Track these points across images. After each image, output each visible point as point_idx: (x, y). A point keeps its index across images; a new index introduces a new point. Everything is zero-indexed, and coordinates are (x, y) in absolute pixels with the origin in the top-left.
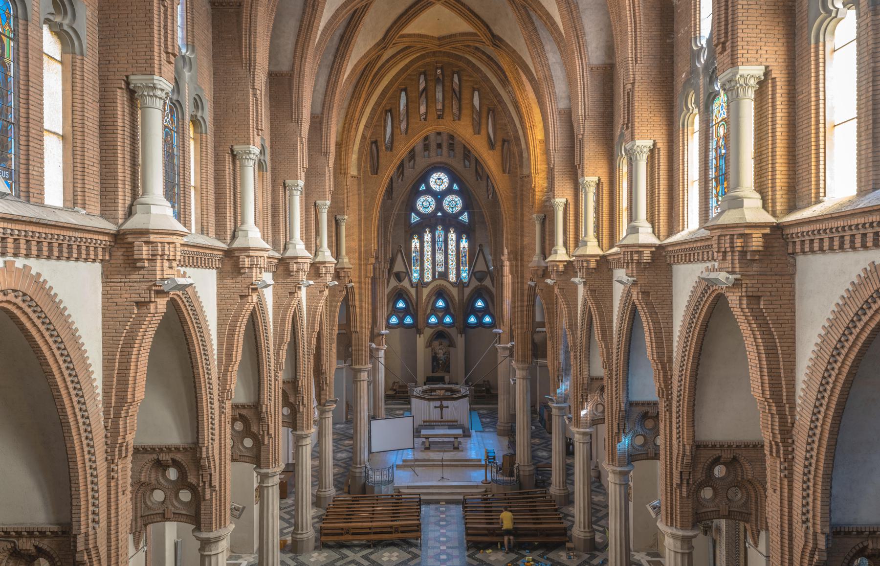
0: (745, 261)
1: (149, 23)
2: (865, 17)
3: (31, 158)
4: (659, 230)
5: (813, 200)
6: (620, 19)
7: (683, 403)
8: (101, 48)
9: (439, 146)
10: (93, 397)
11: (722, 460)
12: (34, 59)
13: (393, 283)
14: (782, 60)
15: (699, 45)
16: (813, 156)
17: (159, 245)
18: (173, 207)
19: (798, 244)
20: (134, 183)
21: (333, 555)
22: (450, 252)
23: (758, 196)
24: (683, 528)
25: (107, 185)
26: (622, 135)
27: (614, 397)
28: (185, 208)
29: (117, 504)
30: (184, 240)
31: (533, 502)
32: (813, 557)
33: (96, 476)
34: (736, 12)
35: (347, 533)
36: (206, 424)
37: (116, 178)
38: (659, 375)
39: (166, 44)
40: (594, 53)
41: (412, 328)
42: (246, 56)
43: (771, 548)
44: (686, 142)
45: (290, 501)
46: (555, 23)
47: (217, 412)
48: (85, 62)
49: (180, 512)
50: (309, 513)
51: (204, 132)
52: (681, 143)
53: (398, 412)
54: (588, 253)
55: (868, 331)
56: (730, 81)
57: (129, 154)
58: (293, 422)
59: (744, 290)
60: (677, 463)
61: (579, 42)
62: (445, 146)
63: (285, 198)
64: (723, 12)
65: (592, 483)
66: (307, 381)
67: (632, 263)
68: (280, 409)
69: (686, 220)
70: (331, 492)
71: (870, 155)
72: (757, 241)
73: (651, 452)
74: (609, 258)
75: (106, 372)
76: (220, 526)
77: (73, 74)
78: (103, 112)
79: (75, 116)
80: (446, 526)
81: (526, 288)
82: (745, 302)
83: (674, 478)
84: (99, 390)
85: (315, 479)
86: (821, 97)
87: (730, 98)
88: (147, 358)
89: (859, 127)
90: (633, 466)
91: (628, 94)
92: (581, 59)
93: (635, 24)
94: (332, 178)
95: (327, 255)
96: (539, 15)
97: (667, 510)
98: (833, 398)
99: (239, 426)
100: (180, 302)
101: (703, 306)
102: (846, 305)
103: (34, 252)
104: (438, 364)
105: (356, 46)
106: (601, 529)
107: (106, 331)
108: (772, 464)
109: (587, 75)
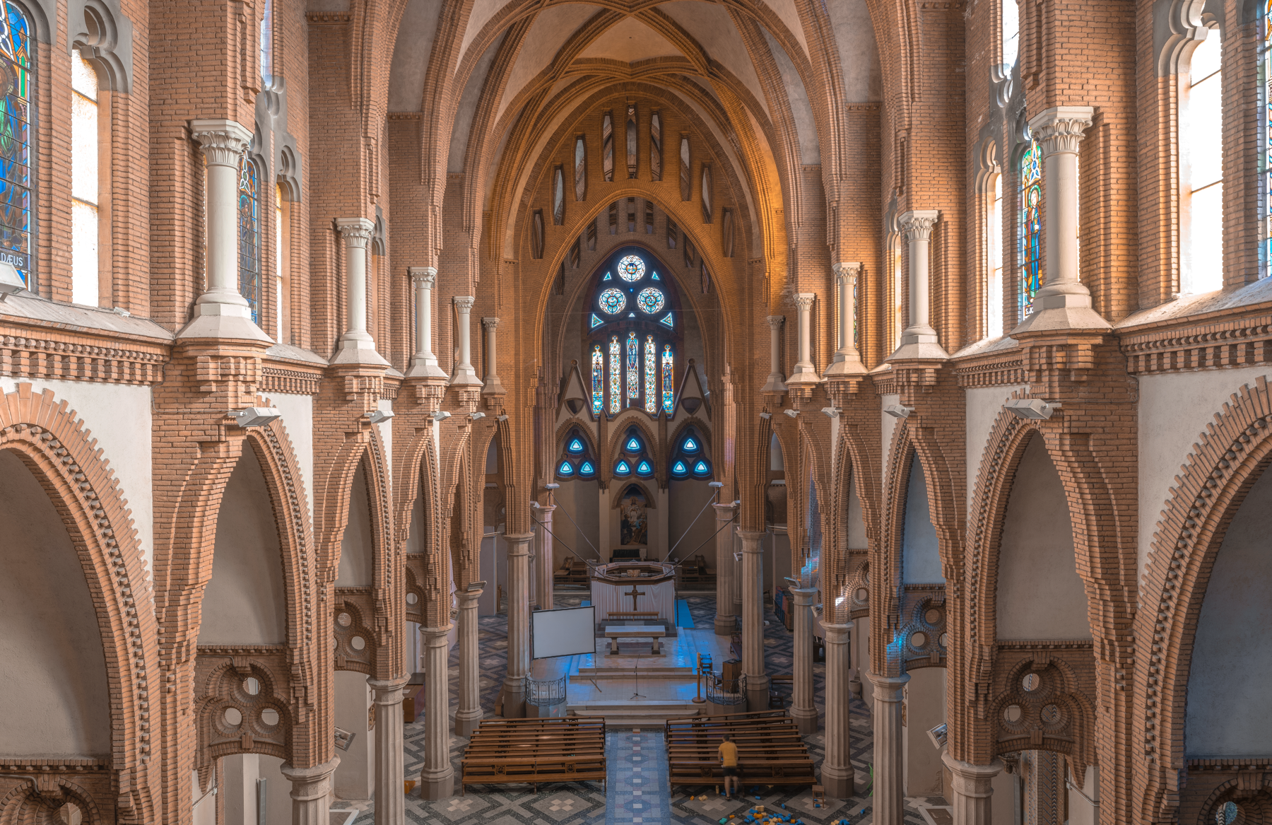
0: (1068, 384)
1: (220, 46)
2: (1233, 39)
3: (54, 238)
4: (947, 340)
5: (1162, 296)
6: (890, 39)
7: (981, 585)
8: (152, 82)
9: (632, 217)
10: (140, 576)
11: (1034, 666)
12: (60, 98)
13: (565, 414)
14: (1118, 99)
15: (1001, 76)
16: (1162, 235)
17: (232, 360)
18: (251, 306)
19: (1142, 359)
20: (198, 273)
21: (480, 802)
22: (647, 370)
23: (1085, 291)
24: (978, 762)
25: (160, 276)
26: (894, 202)
27: (883, 578)
28: (268, 308)
29: (175, 729)
30: (267, 353)
31: (765, 728)
32: (1160, 802)
33: (146, 689)
34: (1053, 30)
35: (500, 772)
36: (298, 616)
37: (172, 265)
38: (947, 546)
39: (244, 76)
40: (853, 86)
41: (592, 479)
42: (356, 91)
43: (1101, 789)
44: (984, 213)
45: (418, 726)
46: (797, 43)
47: (313, 599)
48: (130, 103)
49: (263, 740)
50: (445, 744)
51: (295, 199)
52: (977, 214)
53: (572, 601)
54: (846, 371)
55: (1239, 482)
56: (1045, 128)
57: (190, 231)
58: (422, 613)
59: (1066, 424)
60: (971, 671)
61: (831, 71)
62: (640, 217)
63: (410, 293)
64: (1034, 30)
65: (851, 701)
66: (441, 555)
67: (909, 386)
68: (404, 595)
69: (985, 325)
70: (477, 714)
71: (1242, 234)
72: (1084, 355)
73: (935, 657)
74: (876, 379)
75: (158, 542)
76: (320, 760)
77: (113, 119)
78: (154, 172)
79: (115, 179)
80: (641, 762)
81: (757, 422)
82: (1067, 442)
83: (967, 692)
84: (149, 567)
85: (455, 696)
86: (1173, 151)
87: (1045, 153)
88: (216, 521)
89: (1225, 195)
90: (909, 677)
91: (902, 143)
92: (835, 94)
93: (911, 46)
94: (477, 263)
95: (469, 374)
96: (774, 32)
97: (955, 738)
98: (1190, 578)
99: (345, 619)
100: (261, 442)
101: (1009, 448)
102: (1208, 447)
103: (58, 371)
104: (630, 531)
105: (512, 76)
106: (863, 766)
107: (158, 483)
108: (1104, 671)
109: (843, 117)
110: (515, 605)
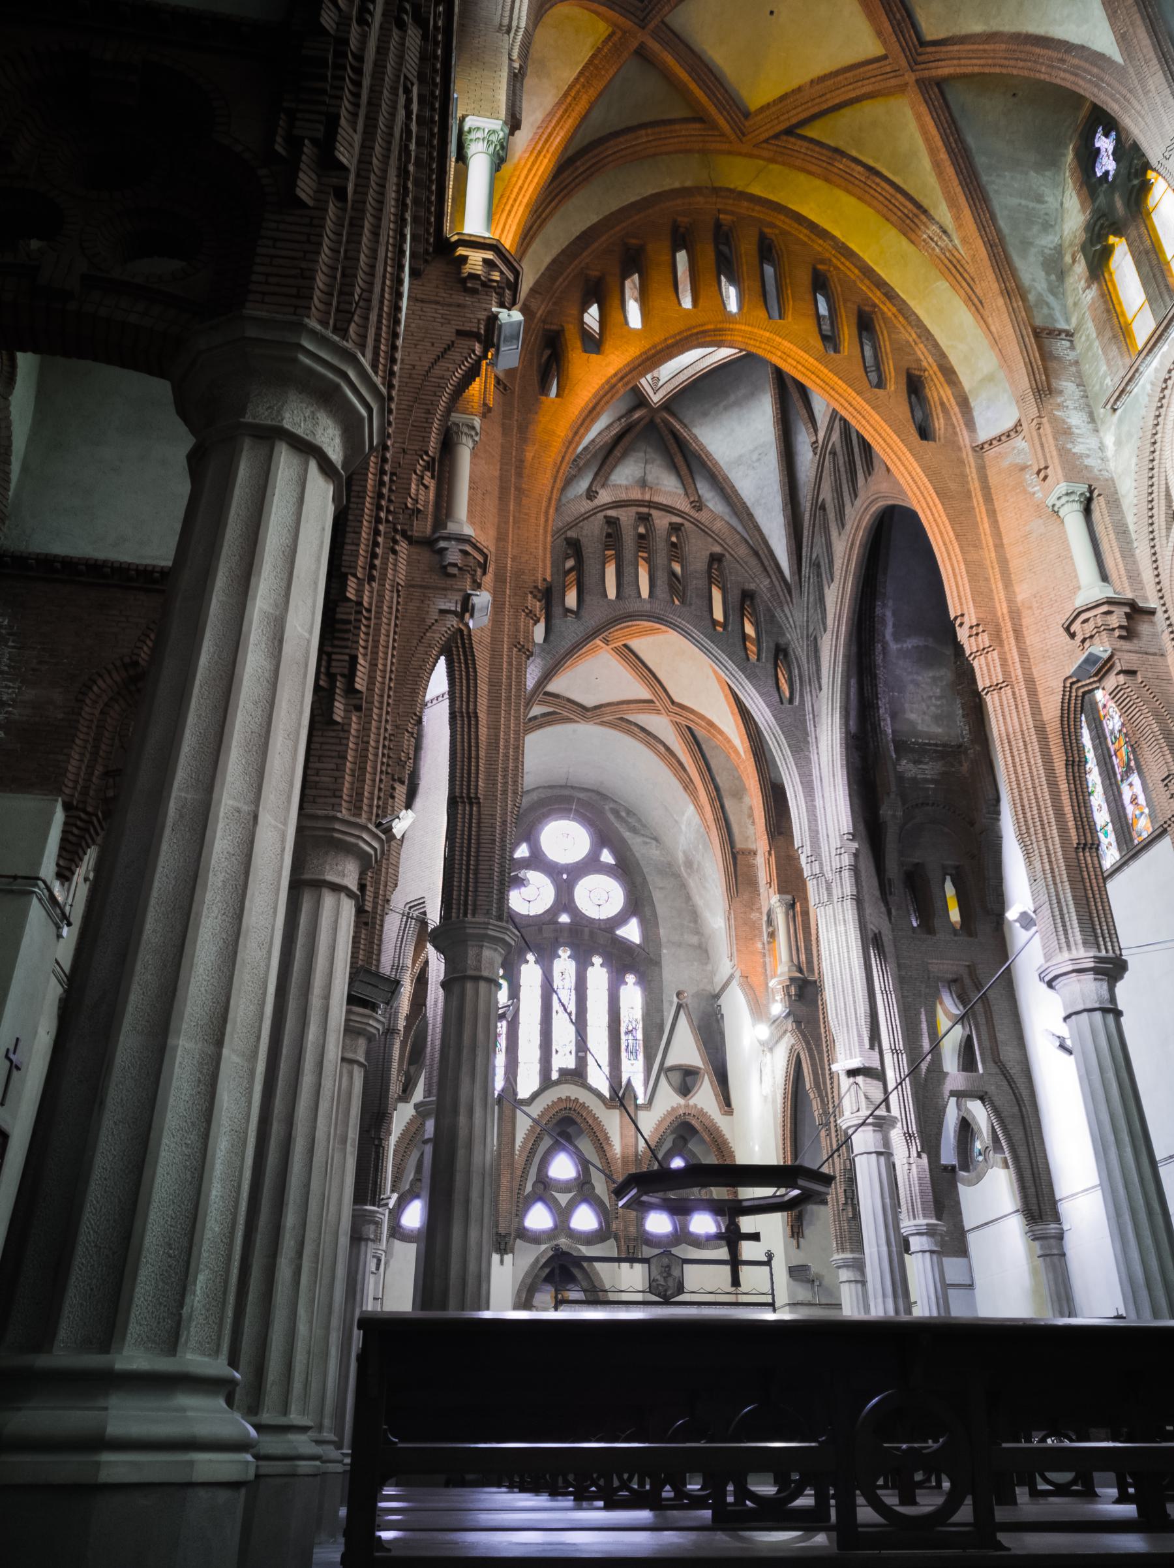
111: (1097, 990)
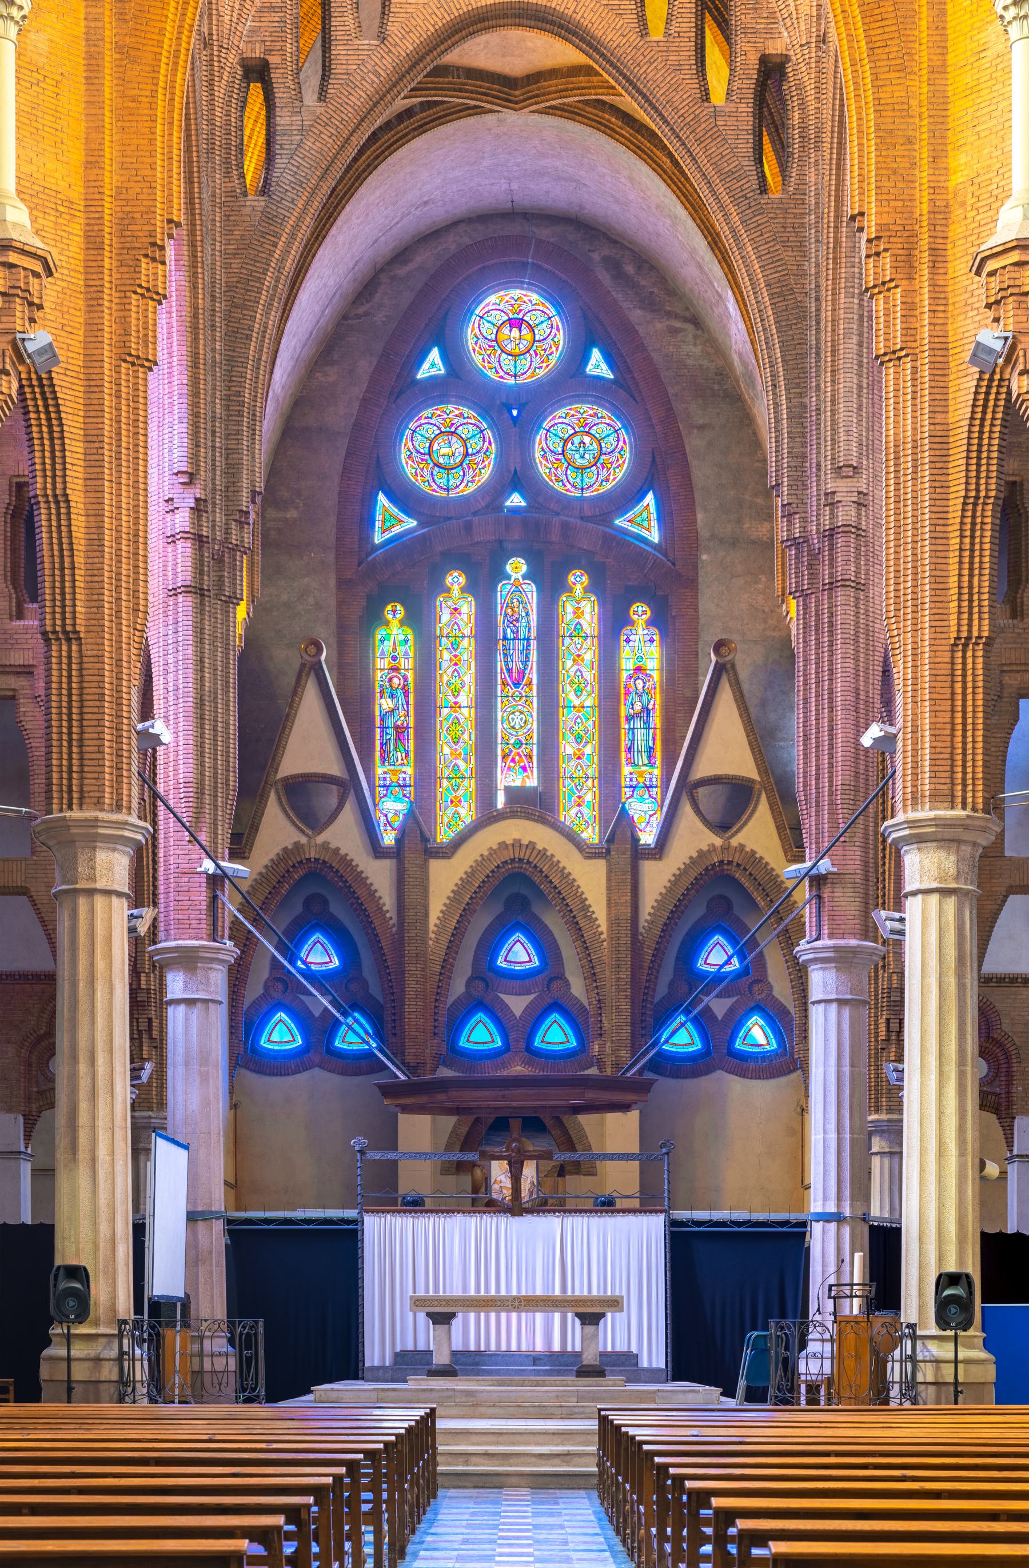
22: (569, 695)
110: (83, 1068)
111: (940, 863)
